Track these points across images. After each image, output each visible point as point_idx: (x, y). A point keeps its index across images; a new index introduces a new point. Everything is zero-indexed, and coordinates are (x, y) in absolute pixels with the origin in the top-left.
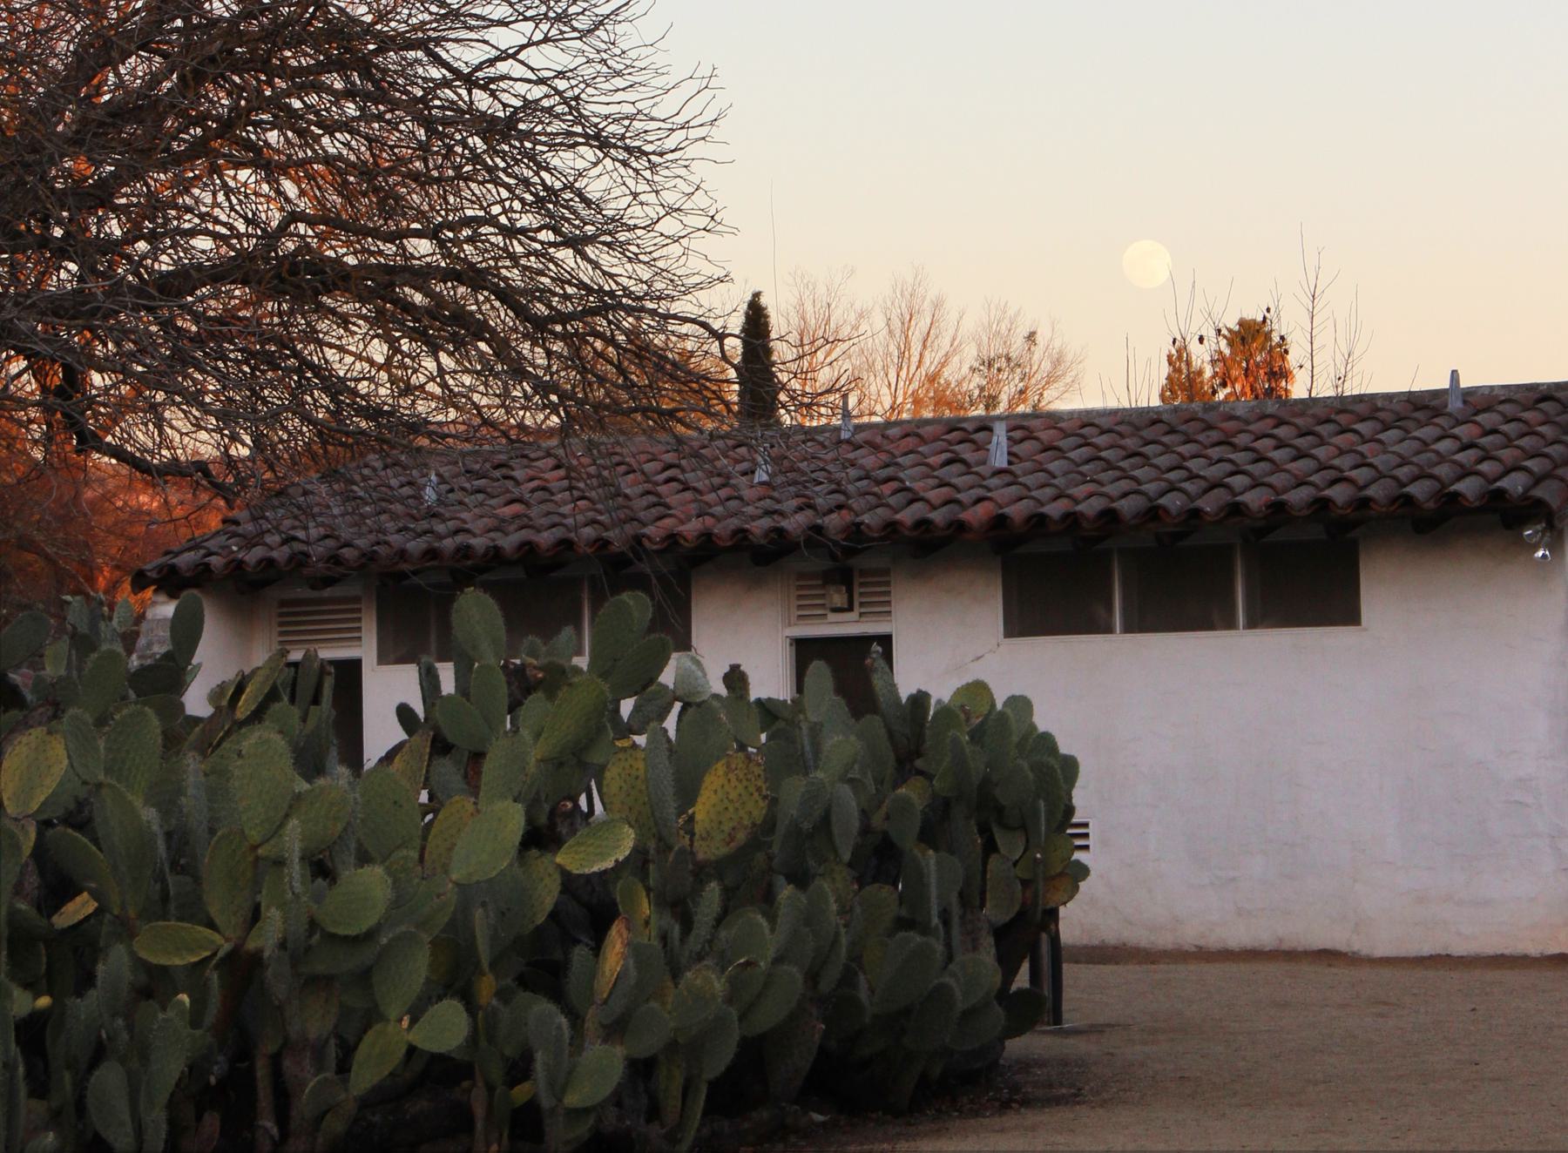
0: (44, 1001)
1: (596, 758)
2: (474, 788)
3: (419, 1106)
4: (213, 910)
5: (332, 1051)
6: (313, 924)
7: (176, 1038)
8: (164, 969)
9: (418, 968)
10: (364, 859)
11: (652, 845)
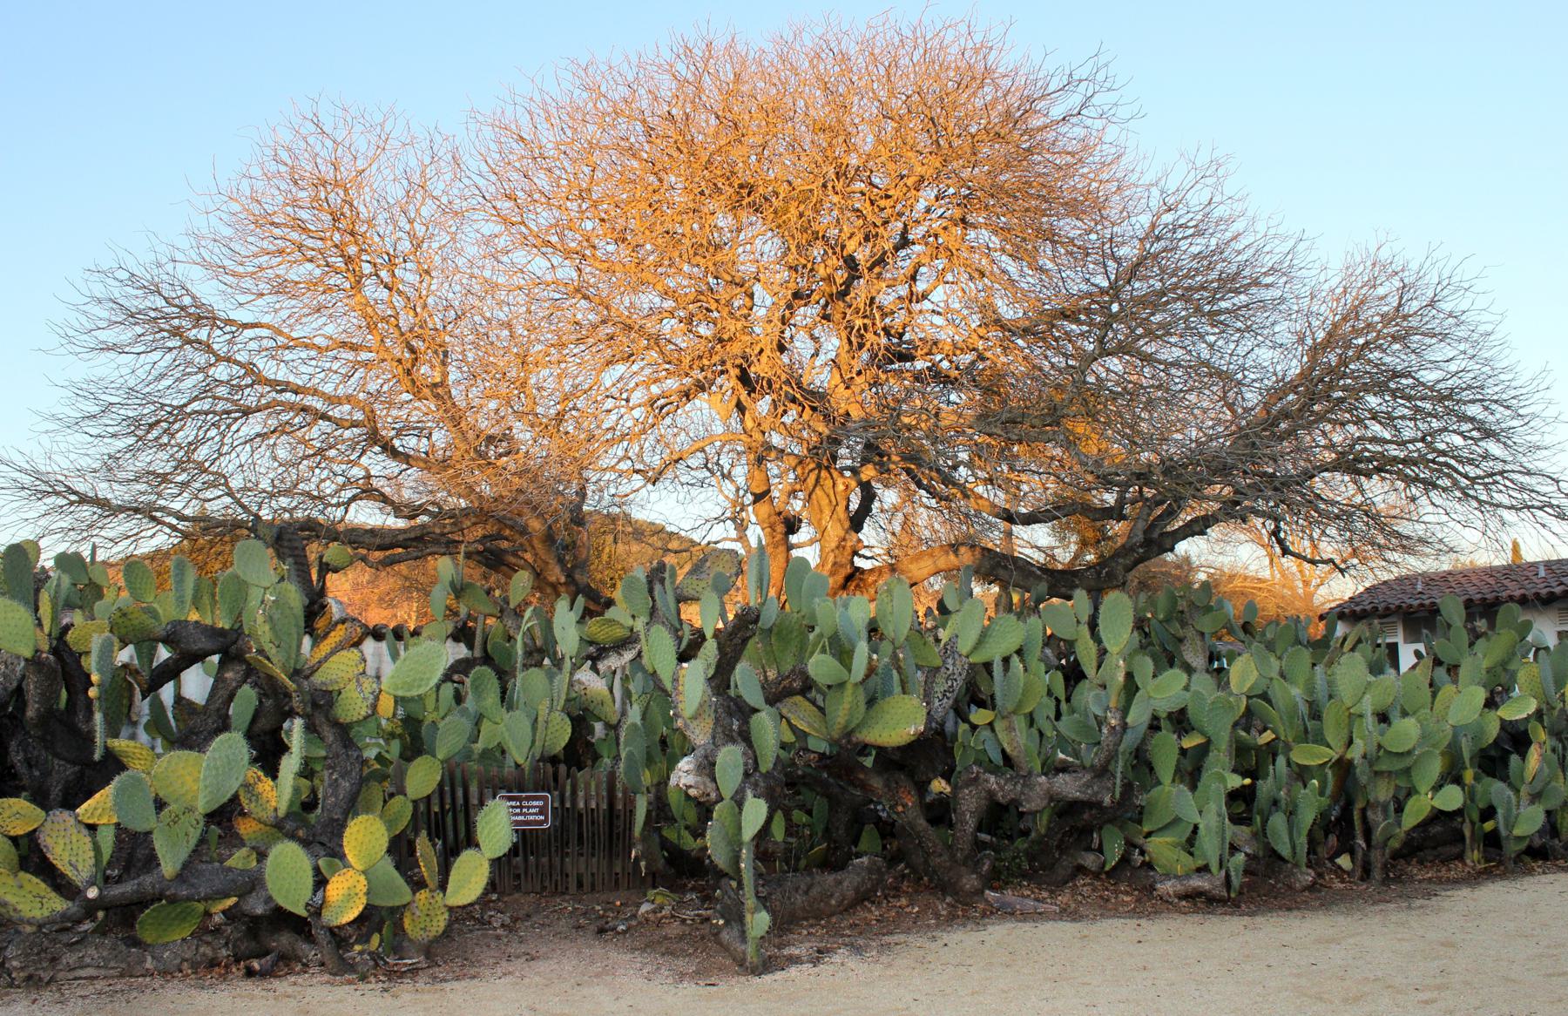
0: (1248, 781)
1: (1512, 667)
2: (1455, 682)
3: (1436, 829)
4: (1329, 740)
5: (1392, 808)
6: (1380, 747)
7: (1311, 803)
8: (1306, 767)
9: (1436, 767)
10: (1405, 714)
11: (1544, 707)
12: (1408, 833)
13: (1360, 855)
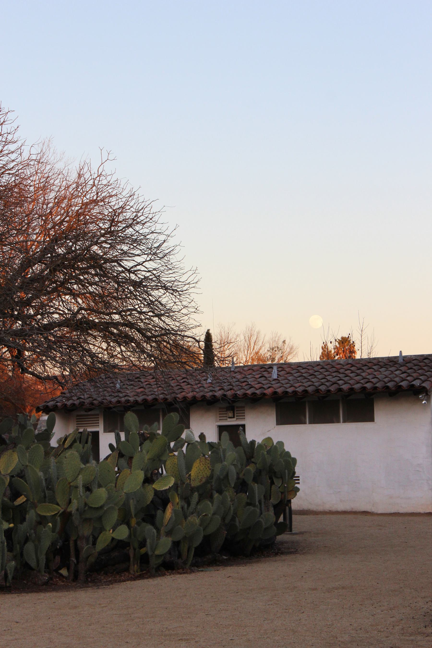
0: (12, 525)
1: (164, 458)
2: (130, 467)
3: (115, 554)
4: (58, 500)
5: (91, 539)
6: (86, 504)
7: (48, 536)
8: (45, 517)
9: (115, 516)
10: (100, 486)
11: (179, 482)
12: (100, 553)
13: (72, 567)
